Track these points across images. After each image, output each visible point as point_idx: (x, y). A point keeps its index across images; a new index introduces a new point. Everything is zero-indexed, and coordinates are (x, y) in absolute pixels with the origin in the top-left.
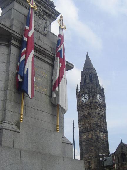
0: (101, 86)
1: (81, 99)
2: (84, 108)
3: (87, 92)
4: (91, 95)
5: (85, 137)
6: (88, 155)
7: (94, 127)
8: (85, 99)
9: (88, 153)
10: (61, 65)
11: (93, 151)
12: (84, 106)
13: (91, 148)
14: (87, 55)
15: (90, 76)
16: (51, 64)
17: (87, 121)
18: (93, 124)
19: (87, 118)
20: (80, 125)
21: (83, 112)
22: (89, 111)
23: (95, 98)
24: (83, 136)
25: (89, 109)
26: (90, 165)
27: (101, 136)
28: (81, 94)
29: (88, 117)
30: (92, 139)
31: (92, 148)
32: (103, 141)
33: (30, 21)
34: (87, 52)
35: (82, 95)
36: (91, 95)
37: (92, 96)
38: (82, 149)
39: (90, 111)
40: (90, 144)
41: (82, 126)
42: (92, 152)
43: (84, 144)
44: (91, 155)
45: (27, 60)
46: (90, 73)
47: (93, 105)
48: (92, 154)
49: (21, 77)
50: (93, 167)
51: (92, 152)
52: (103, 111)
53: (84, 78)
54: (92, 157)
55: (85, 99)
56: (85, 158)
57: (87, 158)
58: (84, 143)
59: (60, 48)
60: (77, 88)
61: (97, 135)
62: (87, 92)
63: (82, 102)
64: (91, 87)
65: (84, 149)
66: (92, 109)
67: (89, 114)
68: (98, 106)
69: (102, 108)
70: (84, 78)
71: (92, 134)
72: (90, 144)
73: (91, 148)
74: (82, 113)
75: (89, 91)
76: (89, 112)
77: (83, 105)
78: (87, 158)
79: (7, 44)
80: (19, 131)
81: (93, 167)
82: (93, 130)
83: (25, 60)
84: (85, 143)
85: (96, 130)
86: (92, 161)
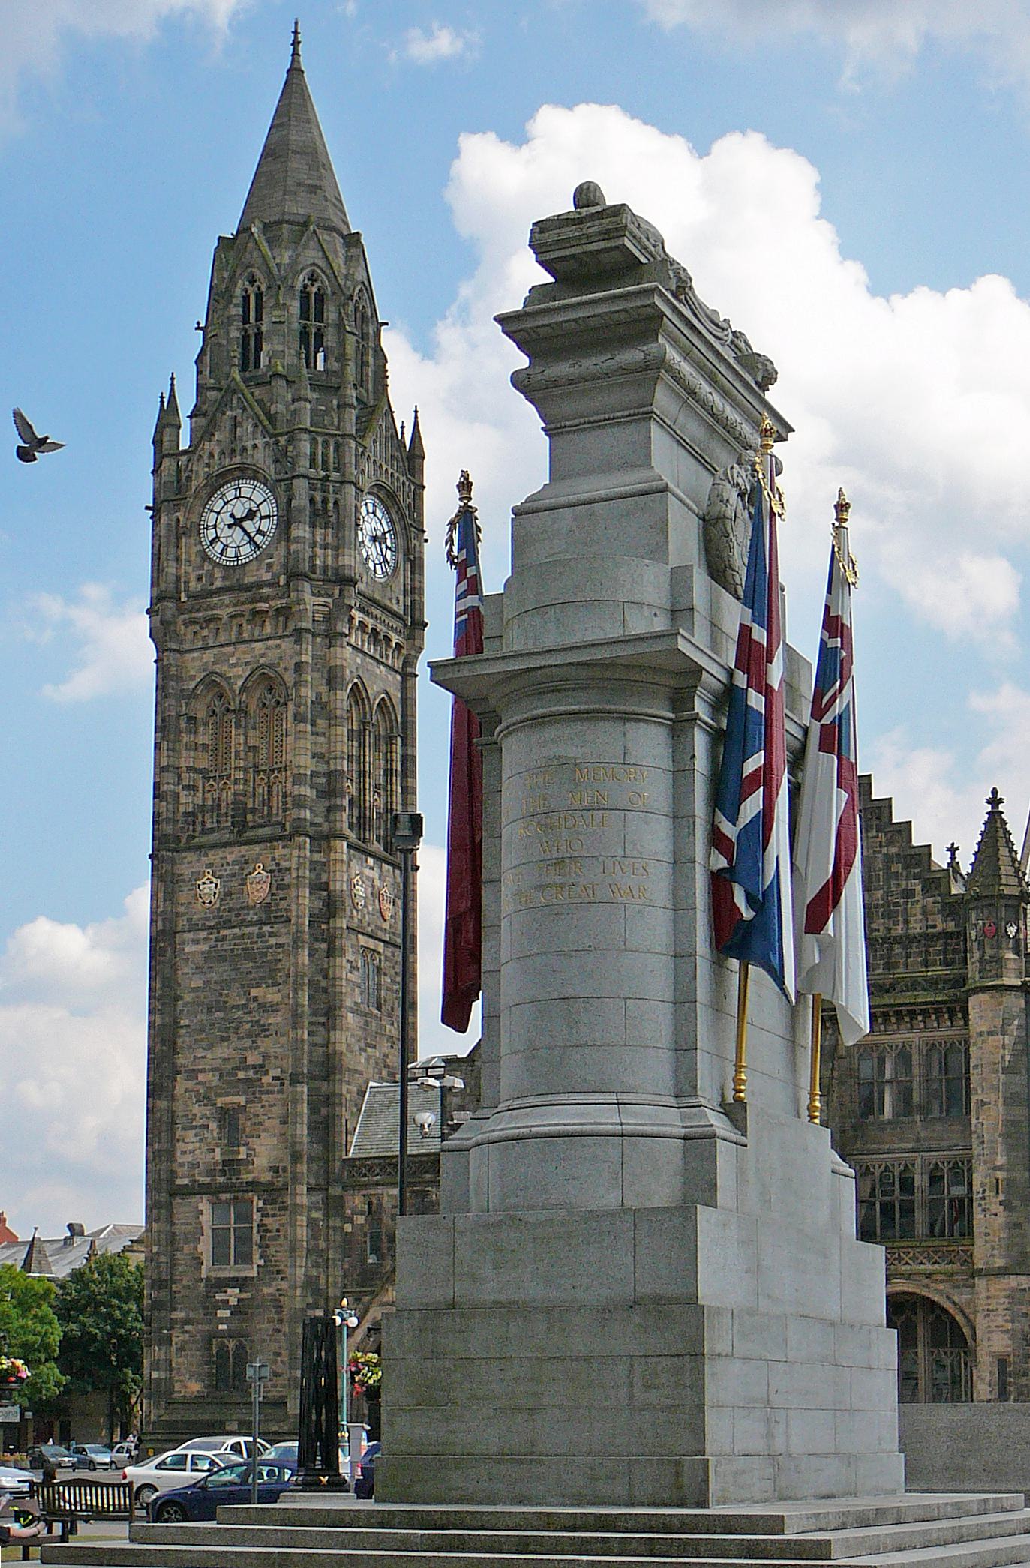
0: (402, 417)
1: (197, 529)
2: (223, 613)
3: (271, 471)
4: (301, 501)
5: (209, 888)
6: (223, 1051)
7: (299, 803)
8: (238, 523)
9: (223, 1039)
10: (845, 796)
11: (274, 1019)
12: (226, 598)
13: (254, 992)
14: (295, 72)
15: (305, 296)
16: (710, 726)
17: (237, 738)
18: (298, 780)
19: (242, 711)
20: (170, 777)
21: (209, 656)
22: (272, 656)
23: (336, 536)
24: (198, 876)
25: (268, 630)
26: (233, 1143)
27: (360, 890)
28: (200, 473)
29: (252, 708)
30: (272, 914)
31: (272, 996)
32: (371, 943)
33: (770, 596)
34: (296, 43)
35: (217, 483)
36: (301, 501)
37: (314, 514)
38: (177, 998)
39: (280, 652)
40: (249, 955)
41: (191, 788)
42: (264, 1030)
43: (193, 947)
44: (253, 1059)
45: (772, 819)
46: (313, 279)
47: (310, 601)
48: (266, 1044)
49: (750, 900)
50: (262, 1161)
51: (264, 1030)
52: (398, 665)
53: (245, 319)
54: (261, 1069)
55: (238, 523)
56: (193, 1074)
57: (213, 1079)
58: (197, 942)
59: (841, 702)
60: (168, 413)
61: (325, 886)
62: (261, 458)
63: (205, 557)
64: (307, 424)
65: (188, 997)
66: (298, 641)
67: (265, 678)
68: (358, 616)
69: (388, 639)
70: (245, 319)
71: (278, 872)
72: (249, 955)
73: (254, 992)
74: (195, 665)
75: (281, 456)
76: (270, 666)
77: (218, 584)
78: (213, 1079)
79: (672, 716)
80: (743, 1140)
81: (262, 1161)
82: (290, 837)
83: (767, 816)
84: (205, 947)
85: (323, 839)
86: (257, 1108)
